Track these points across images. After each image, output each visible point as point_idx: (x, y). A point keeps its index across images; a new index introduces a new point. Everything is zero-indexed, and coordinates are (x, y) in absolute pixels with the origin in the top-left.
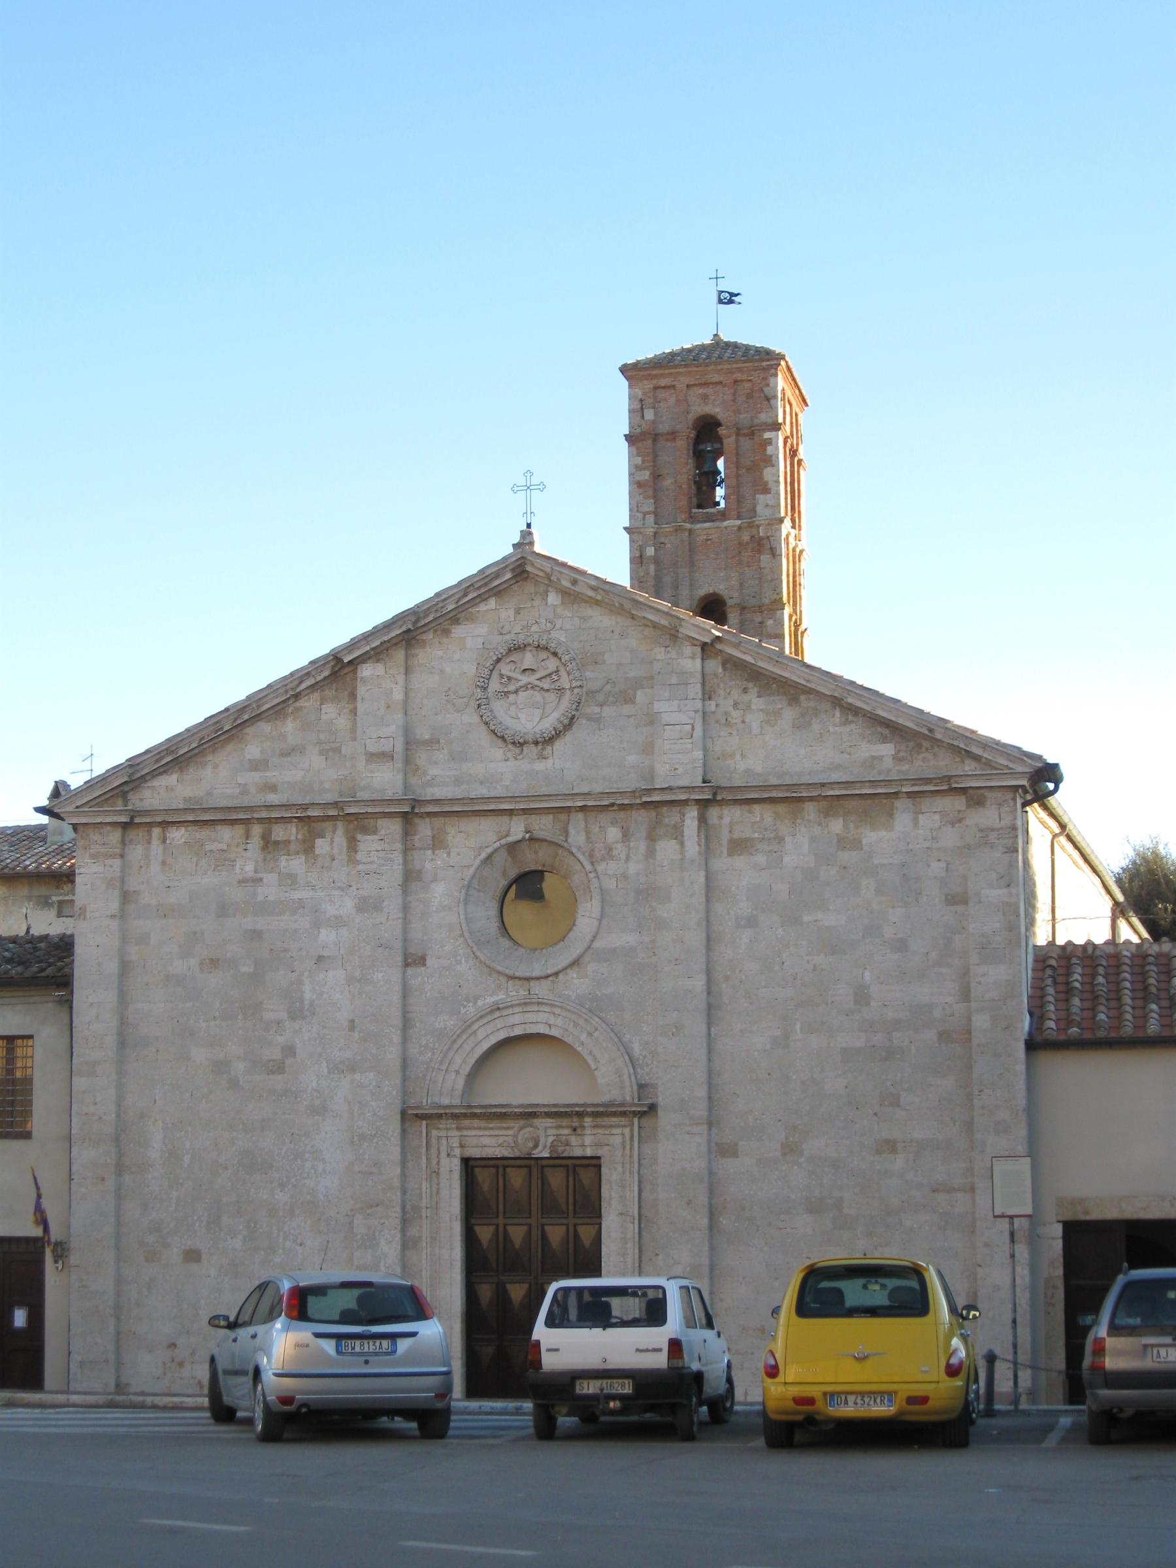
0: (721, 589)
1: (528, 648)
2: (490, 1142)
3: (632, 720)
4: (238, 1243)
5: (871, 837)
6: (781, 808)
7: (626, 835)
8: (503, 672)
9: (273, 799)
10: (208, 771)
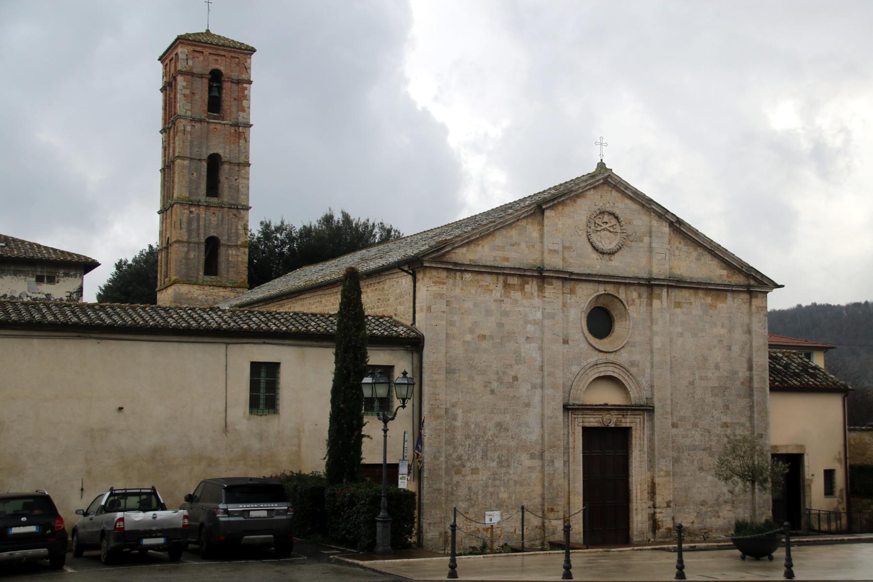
0: (221, 152)
2: (593, 421)
4: (494, 464)
5: (720, 305)
6: (691, 291)
7: (640, 296)
9: (506, 264)
10: (480, 248)
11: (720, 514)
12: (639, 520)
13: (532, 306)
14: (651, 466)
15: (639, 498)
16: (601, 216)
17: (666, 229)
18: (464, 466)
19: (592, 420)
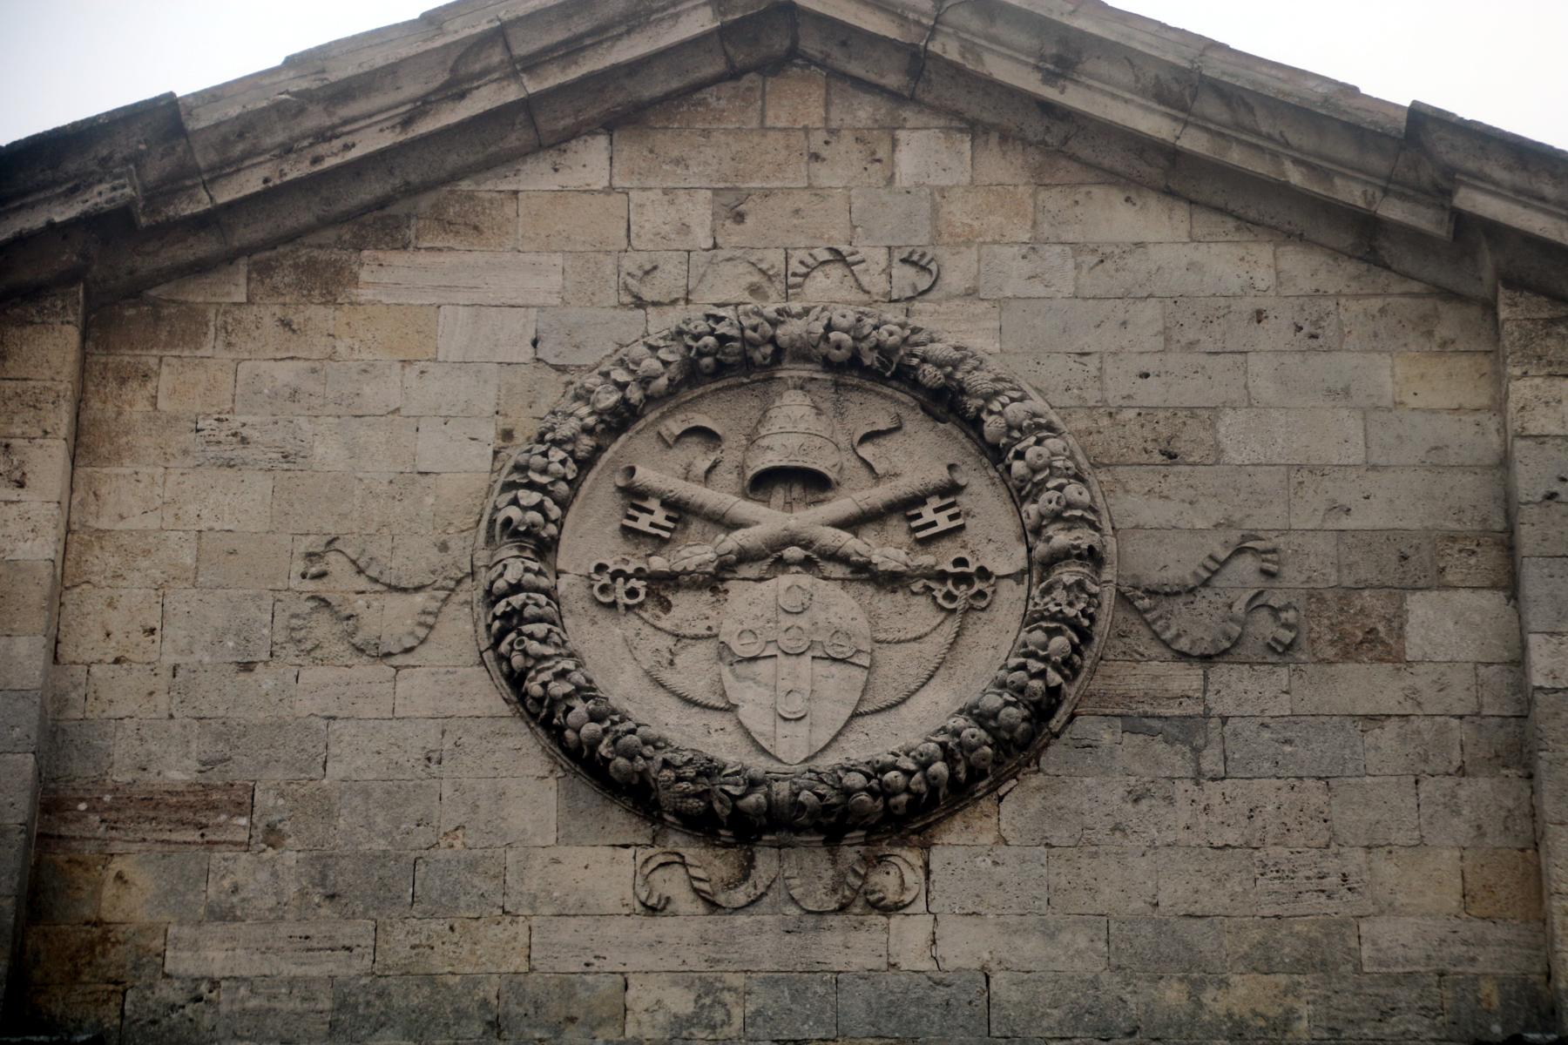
1: (792, 371)
3: (1387, 736)
8: (646, 476)
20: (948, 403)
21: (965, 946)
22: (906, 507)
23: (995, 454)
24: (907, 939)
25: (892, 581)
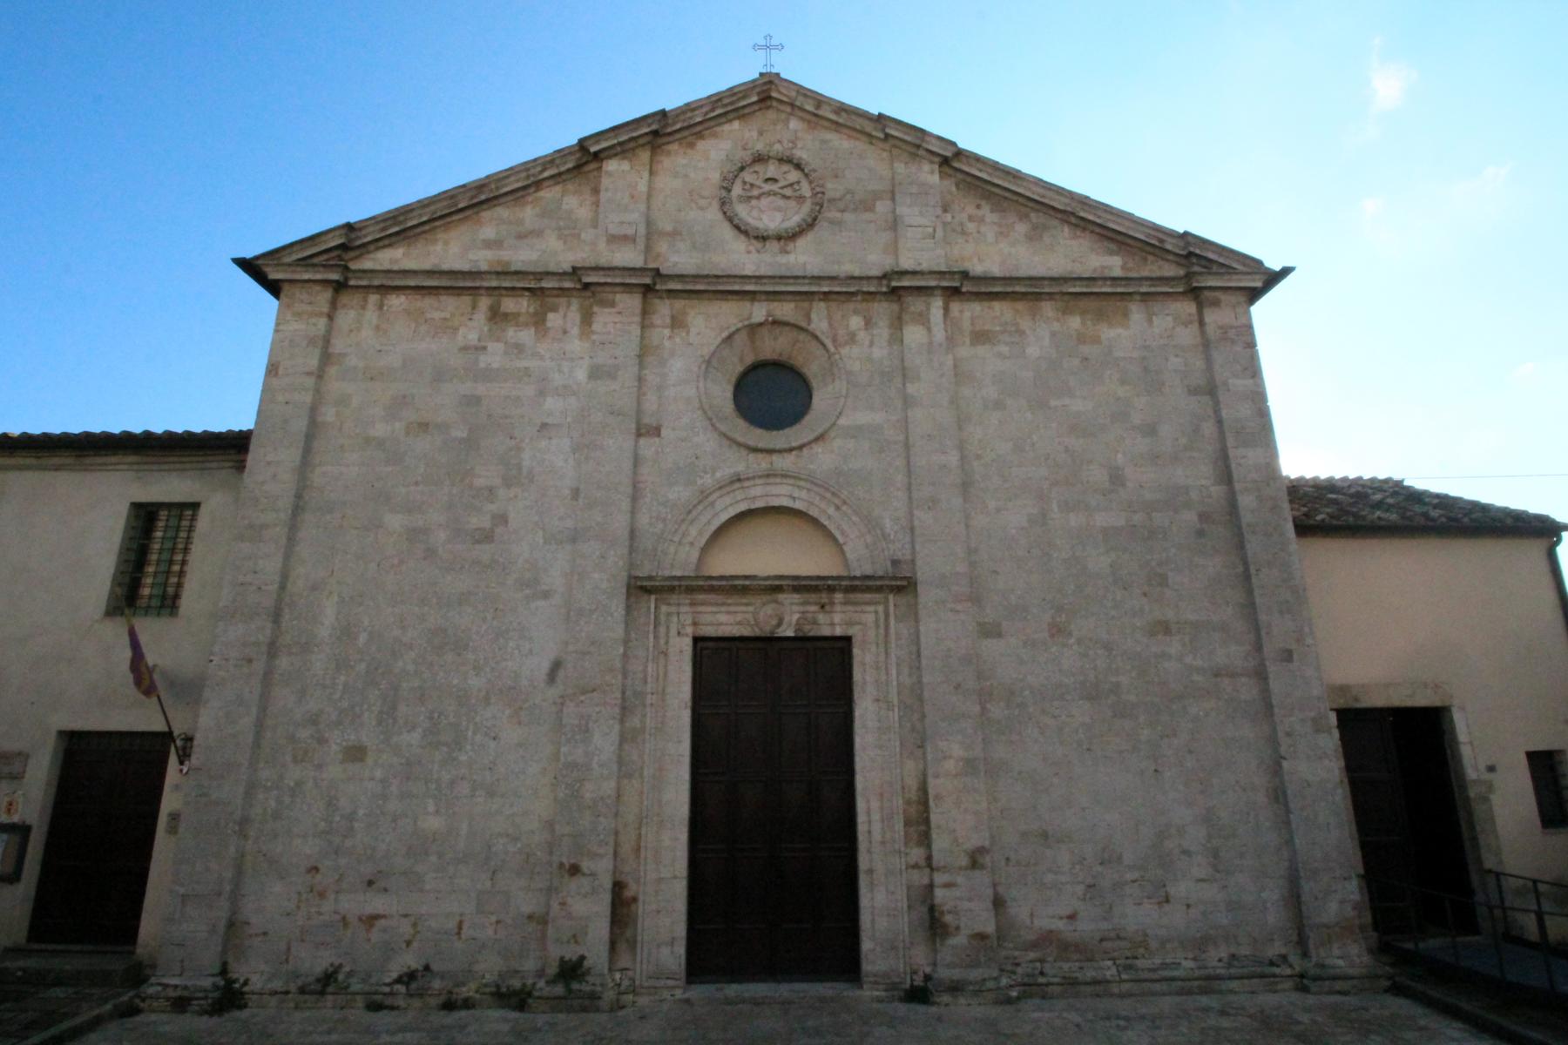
2: (727, 620)
4: (415, 737)
5: (1108, 333)
7: (868, 323)
10: (439, 247)
11: (1172, 891)
12: (882, 904)
13: (569, 358)
14: (918, 741)
15: (877, 836)
16: (757, 167)
17: (929, 175)
18: (322, 741)
19: (723, 618)
20: (798, 166)
21: (802, 259)
22: (791, 185)
23: (806, 175)
24: (791, 258)
25: (788, 198)
